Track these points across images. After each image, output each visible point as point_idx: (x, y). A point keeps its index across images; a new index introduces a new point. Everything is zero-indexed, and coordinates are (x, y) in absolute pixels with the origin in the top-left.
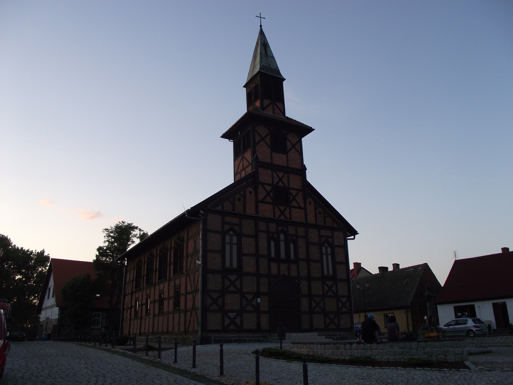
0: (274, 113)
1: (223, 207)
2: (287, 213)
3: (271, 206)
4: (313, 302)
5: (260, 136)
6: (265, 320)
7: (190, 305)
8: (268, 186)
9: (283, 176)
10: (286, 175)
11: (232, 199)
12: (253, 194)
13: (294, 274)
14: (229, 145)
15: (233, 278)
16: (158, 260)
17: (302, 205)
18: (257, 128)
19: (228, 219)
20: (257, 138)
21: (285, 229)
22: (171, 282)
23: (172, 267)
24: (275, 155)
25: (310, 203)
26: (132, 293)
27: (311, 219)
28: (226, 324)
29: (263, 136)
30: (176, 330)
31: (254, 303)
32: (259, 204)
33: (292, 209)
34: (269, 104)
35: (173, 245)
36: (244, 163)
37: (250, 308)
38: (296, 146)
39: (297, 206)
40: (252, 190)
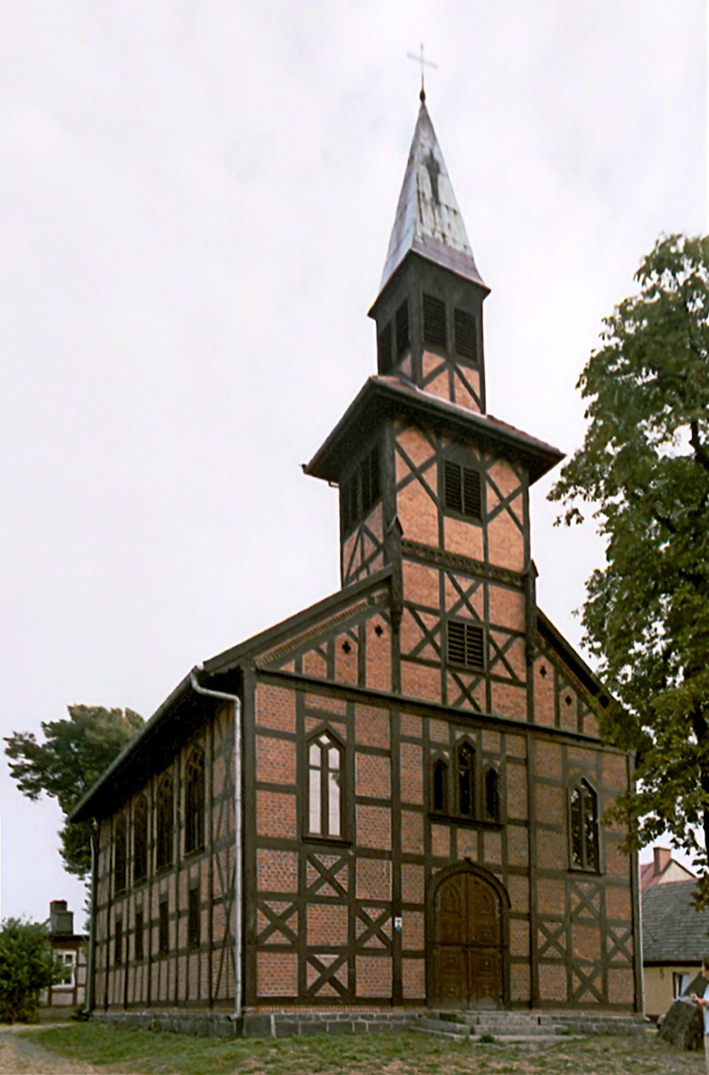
0: (452, 398)
1: (298, 668)
2: (452, 598)
3: (436, 672)
4: (540, 934)
6: (414, 971)
7: (219, 934)
8: (431, 616)
9: (472, 590)
10: (481, 587)
11: (324, 646)
12: (386, 635)
13: (492, 858)
14: (327, 496)
15: (328, 861)
16: (155, 816)
18: (399, 439)
19: (315, 701)
20: (401, 471)
21: (473, 736)
22: (182, 873)
23: (183, 832)
25: (543, 672)
26: (110, 903)
27: (544, 717)
28: (310, 982)
29: (417, 464)
30: (193, 997)
31: (386, 929)
33: (493, 685)
35: (183, 775)
36: (366, 545)
37: (374, 942)
38: (512, 504)
39: (509, 676)
40: (384, 624)
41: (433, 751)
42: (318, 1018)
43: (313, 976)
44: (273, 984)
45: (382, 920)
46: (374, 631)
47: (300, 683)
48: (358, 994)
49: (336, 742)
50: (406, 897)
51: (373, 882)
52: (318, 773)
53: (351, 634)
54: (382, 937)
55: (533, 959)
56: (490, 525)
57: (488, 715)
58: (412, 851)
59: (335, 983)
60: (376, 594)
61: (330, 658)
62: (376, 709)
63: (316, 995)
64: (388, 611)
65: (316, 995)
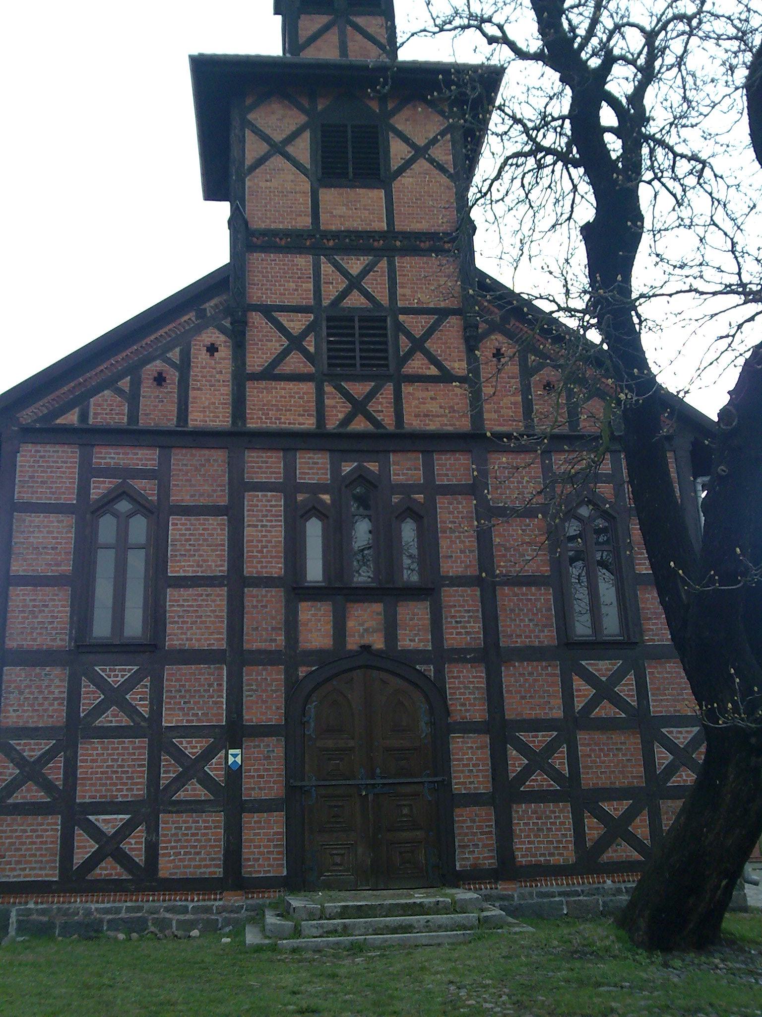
1: (84, 416)
3: (309, 388)
5: (285, 353)
6: (265, 843)
11: (125, 383)
12: (225, 353)
17: (459, 367)
18: (250, 117)
19: (108, 456)
21: (373, 467)
24: (327, 196)
31: (214, 770)
32: (249, 384)
33: (407, 389)
34: (326, 28)
37: (194, 790)
39: (434, 371)
40: (218, 338)
41: (300, 497)
42: (88, 913)
43: (85, 847)
44: (18, 862)
45: (207, 755)
46: (204, 351)
47: (88, 436)
48: (163, 874)
49: (142, 507)
50: (252, 715)
51: (193, 699)
52: (111, 553)
53: (169, 361)
54: (207, 781)
55: (504, 795)
56: (395, 185)
57: (344, 61)
58: (263, 646)
59: (123, 859)
60: (209, 306)
61: (133, 399)
62: (206, 452)
63: (89, 877)
64: (227, 323)
65: (89, 877)
